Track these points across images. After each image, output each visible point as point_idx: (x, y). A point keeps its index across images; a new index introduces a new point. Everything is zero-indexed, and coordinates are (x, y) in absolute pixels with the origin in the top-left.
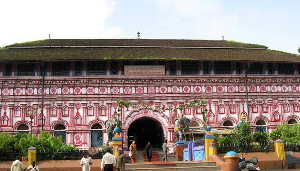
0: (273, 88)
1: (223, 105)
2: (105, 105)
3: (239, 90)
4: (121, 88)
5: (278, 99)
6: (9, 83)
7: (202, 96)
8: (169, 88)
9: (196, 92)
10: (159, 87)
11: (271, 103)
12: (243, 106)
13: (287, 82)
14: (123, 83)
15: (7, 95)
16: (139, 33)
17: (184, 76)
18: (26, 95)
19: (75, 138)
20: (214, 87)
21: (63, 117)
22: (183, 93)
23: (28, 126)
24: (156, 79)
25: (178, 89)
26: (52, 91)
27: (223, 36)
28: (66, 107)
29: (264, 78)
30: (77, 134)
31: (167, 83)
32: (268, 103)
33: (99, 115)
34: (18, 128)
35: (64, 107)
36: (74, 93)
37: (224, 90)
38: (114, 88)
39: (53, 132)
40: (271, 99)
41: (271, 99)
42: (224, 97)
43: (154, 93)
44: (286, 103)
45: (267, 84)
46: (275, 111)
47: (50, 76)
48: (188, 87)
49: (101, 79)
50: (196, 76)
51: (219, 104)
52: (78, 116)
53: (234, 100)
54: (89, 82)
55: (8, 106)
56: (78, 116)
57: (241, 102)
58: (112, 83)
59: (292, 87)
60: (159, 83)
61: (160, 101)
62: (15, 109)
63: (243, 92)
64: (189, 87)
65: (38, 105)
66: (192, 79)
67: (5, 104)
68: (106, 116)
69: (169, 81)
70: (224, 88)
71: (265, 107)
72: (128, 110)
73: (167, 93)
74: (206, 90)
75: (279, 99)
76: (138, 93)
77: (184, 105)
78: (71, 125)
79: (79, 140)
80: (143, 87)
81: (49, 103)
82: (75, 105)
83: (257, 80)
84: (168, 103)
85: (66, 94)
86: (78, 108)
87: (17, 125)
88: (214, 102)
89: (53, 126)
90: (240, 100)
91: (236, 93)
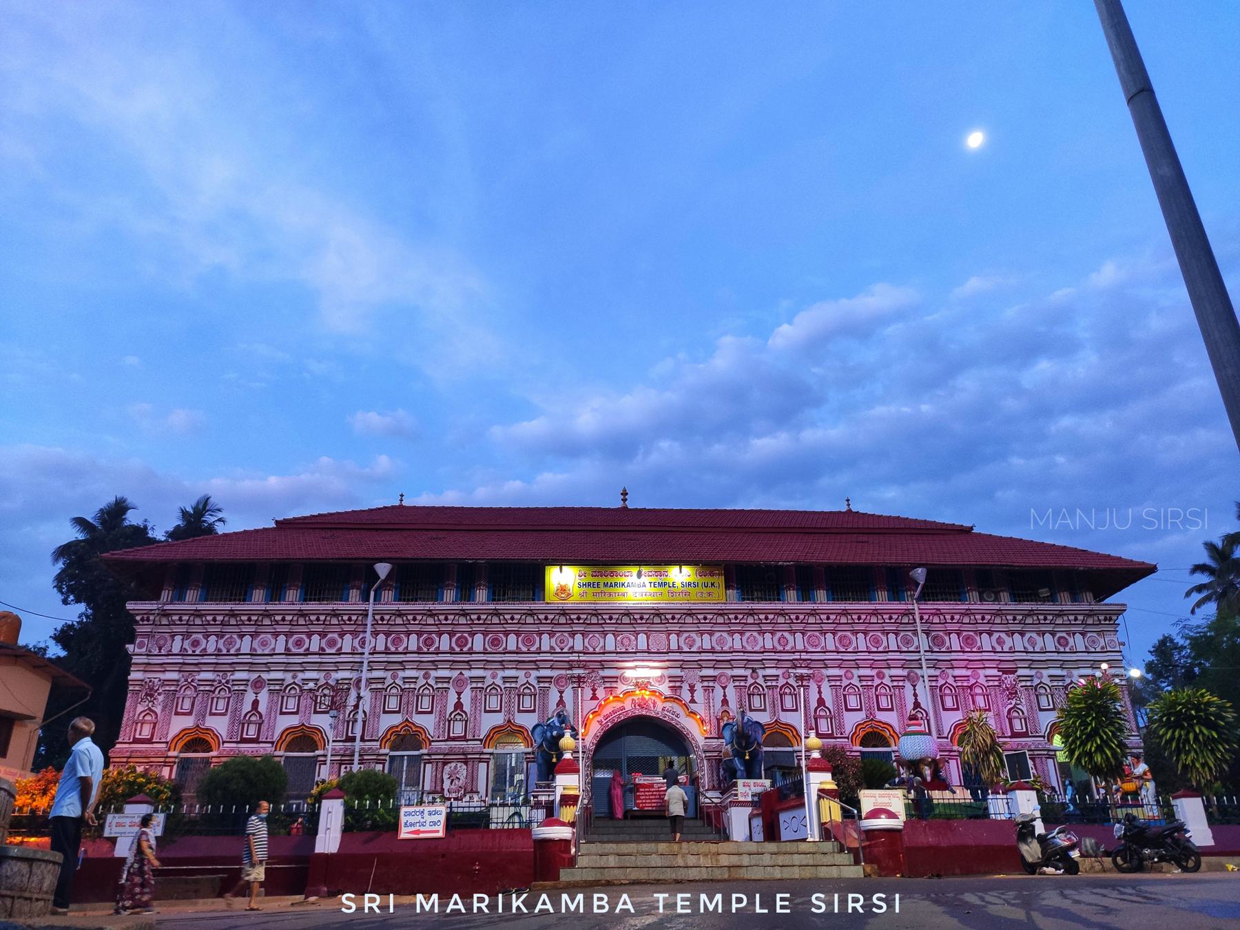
0: (998, 639)
1: (498, 686)
2: (534, 682)
3: (962, 645)
4: (578, 637)
5: (1016, 671)
6: (276, 621)
7: (503, 661)
8: (706, 637)
9: (457, 649)
10: (679, 634)
11: (996, 683)
12: (915, 690)
13: (946, 623)
14: (185, 625)
15: (266, 652)
16: (625, 494)
17: (746, 606)
18: (218, 653)
19: (445, 776)
20: (951, 635)
21: (751, 713)
22: (713, 651)
23: (315, 742)
24: (732, 611)
25: (760, 638)
26: (393, 642)
27: (402, 496)
28: (427, 686)
29: (938, 612)
30: (453, 765)
31: (700, 623)
32: (986, 685)
33: (278, 712)
34: (287, 746)
35: (522, 685)
36: (552, 647)
37: (472, 644)
38: (558, 634)
39: (388, 758)
40: (995, 672)
41: (995, 672)
42: (888, 664)
43: (634, 650)
44: (1041, 682)
45: (825, 627)
46: (1012, 706)
47: (887, 602)
48: (755, 634)
49: (491, 611)
50: (778, 606)
51: (845, 682)
52: (822, 707)
53: (886, 672)
54: (300, 619)
55: (267, 682)
56: (458, 714)
57: (908, 677)
58: (357, 623)
59: (1056, 638)
60: (678, 623)
61: (682, 674)
62: (284, 692)
63: (910, 649)
64: (470, 637)
65: (352, 682)
66: (766, 612)
67: (461, 673)
68: (796, 713)
69: (705, 618)
70: (857, 638)
71: (980, 694)
72: (594, 698)
73: (1012, 651)
74: (869, 645)
75: (1020, 672)
76: (624, 650)
77: (748, 685)
78: (474, 736)
79: (456, 782)
80: (637, 633)
81: (480, 673)
82: (451, 681)
83: (948, 617)
84: (703, 679)
85: (461, 650)
86: (914, 684)
87: (286, 737)
88: (830, 678)
89: (386, 743)
90: (905, 673)
91: (670, 652)
